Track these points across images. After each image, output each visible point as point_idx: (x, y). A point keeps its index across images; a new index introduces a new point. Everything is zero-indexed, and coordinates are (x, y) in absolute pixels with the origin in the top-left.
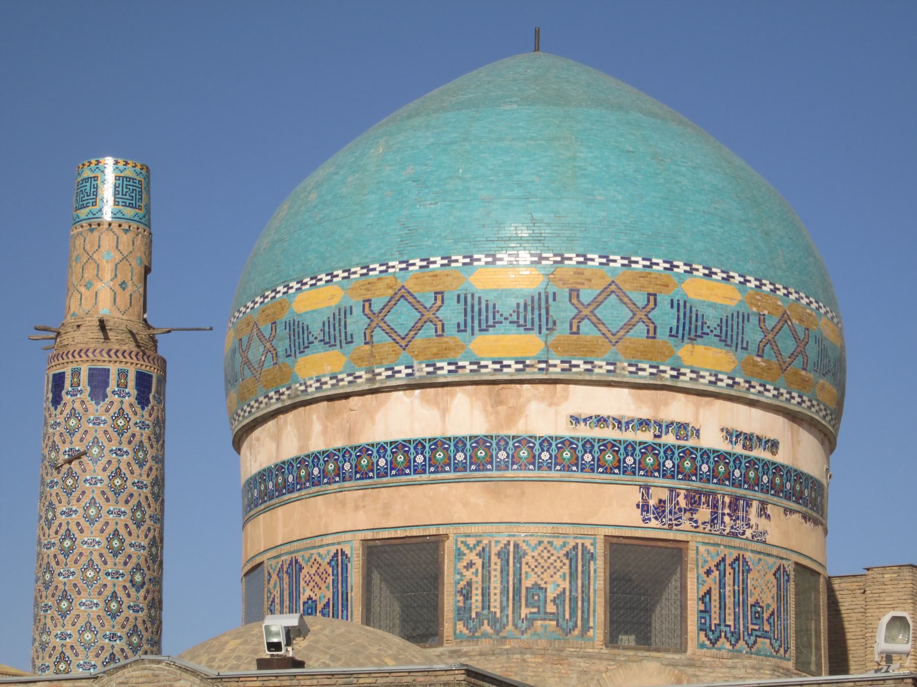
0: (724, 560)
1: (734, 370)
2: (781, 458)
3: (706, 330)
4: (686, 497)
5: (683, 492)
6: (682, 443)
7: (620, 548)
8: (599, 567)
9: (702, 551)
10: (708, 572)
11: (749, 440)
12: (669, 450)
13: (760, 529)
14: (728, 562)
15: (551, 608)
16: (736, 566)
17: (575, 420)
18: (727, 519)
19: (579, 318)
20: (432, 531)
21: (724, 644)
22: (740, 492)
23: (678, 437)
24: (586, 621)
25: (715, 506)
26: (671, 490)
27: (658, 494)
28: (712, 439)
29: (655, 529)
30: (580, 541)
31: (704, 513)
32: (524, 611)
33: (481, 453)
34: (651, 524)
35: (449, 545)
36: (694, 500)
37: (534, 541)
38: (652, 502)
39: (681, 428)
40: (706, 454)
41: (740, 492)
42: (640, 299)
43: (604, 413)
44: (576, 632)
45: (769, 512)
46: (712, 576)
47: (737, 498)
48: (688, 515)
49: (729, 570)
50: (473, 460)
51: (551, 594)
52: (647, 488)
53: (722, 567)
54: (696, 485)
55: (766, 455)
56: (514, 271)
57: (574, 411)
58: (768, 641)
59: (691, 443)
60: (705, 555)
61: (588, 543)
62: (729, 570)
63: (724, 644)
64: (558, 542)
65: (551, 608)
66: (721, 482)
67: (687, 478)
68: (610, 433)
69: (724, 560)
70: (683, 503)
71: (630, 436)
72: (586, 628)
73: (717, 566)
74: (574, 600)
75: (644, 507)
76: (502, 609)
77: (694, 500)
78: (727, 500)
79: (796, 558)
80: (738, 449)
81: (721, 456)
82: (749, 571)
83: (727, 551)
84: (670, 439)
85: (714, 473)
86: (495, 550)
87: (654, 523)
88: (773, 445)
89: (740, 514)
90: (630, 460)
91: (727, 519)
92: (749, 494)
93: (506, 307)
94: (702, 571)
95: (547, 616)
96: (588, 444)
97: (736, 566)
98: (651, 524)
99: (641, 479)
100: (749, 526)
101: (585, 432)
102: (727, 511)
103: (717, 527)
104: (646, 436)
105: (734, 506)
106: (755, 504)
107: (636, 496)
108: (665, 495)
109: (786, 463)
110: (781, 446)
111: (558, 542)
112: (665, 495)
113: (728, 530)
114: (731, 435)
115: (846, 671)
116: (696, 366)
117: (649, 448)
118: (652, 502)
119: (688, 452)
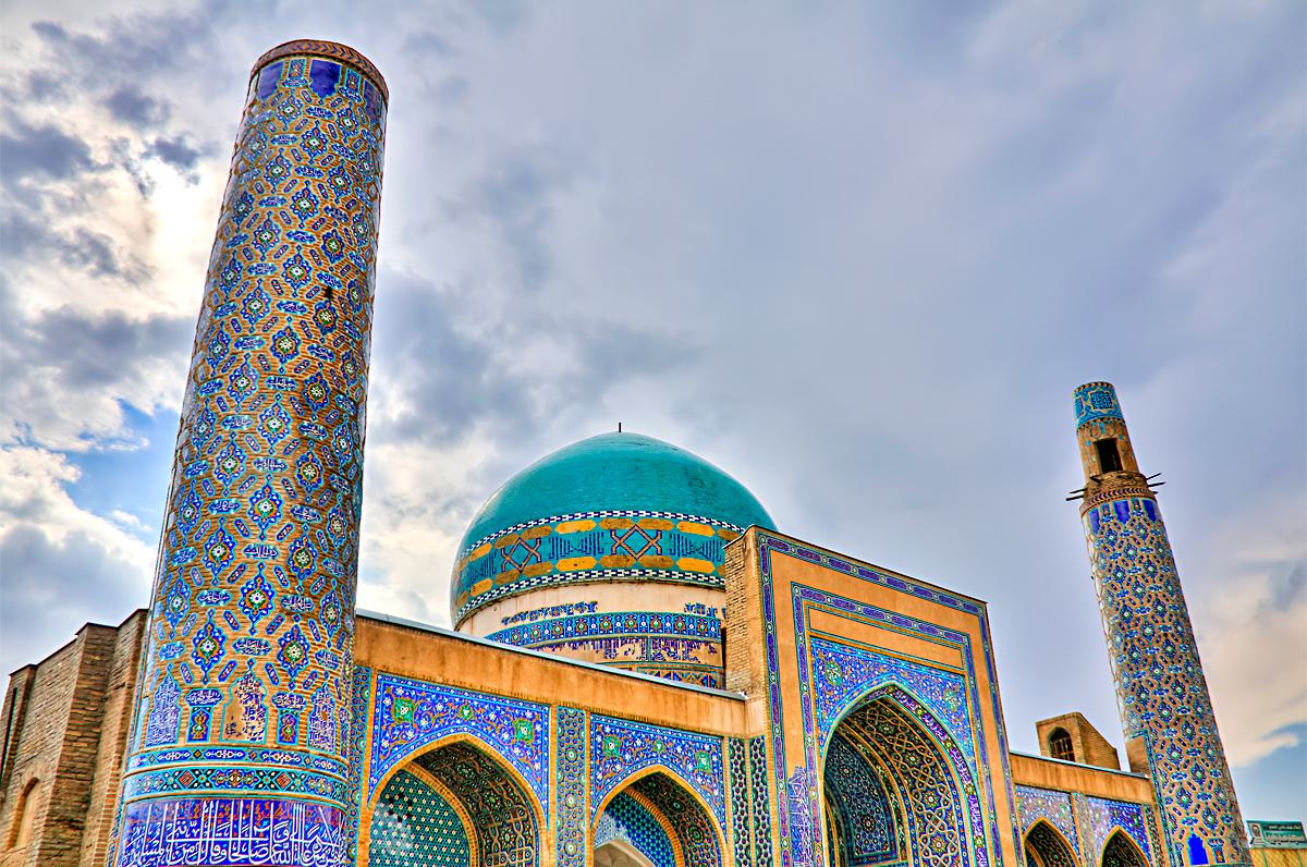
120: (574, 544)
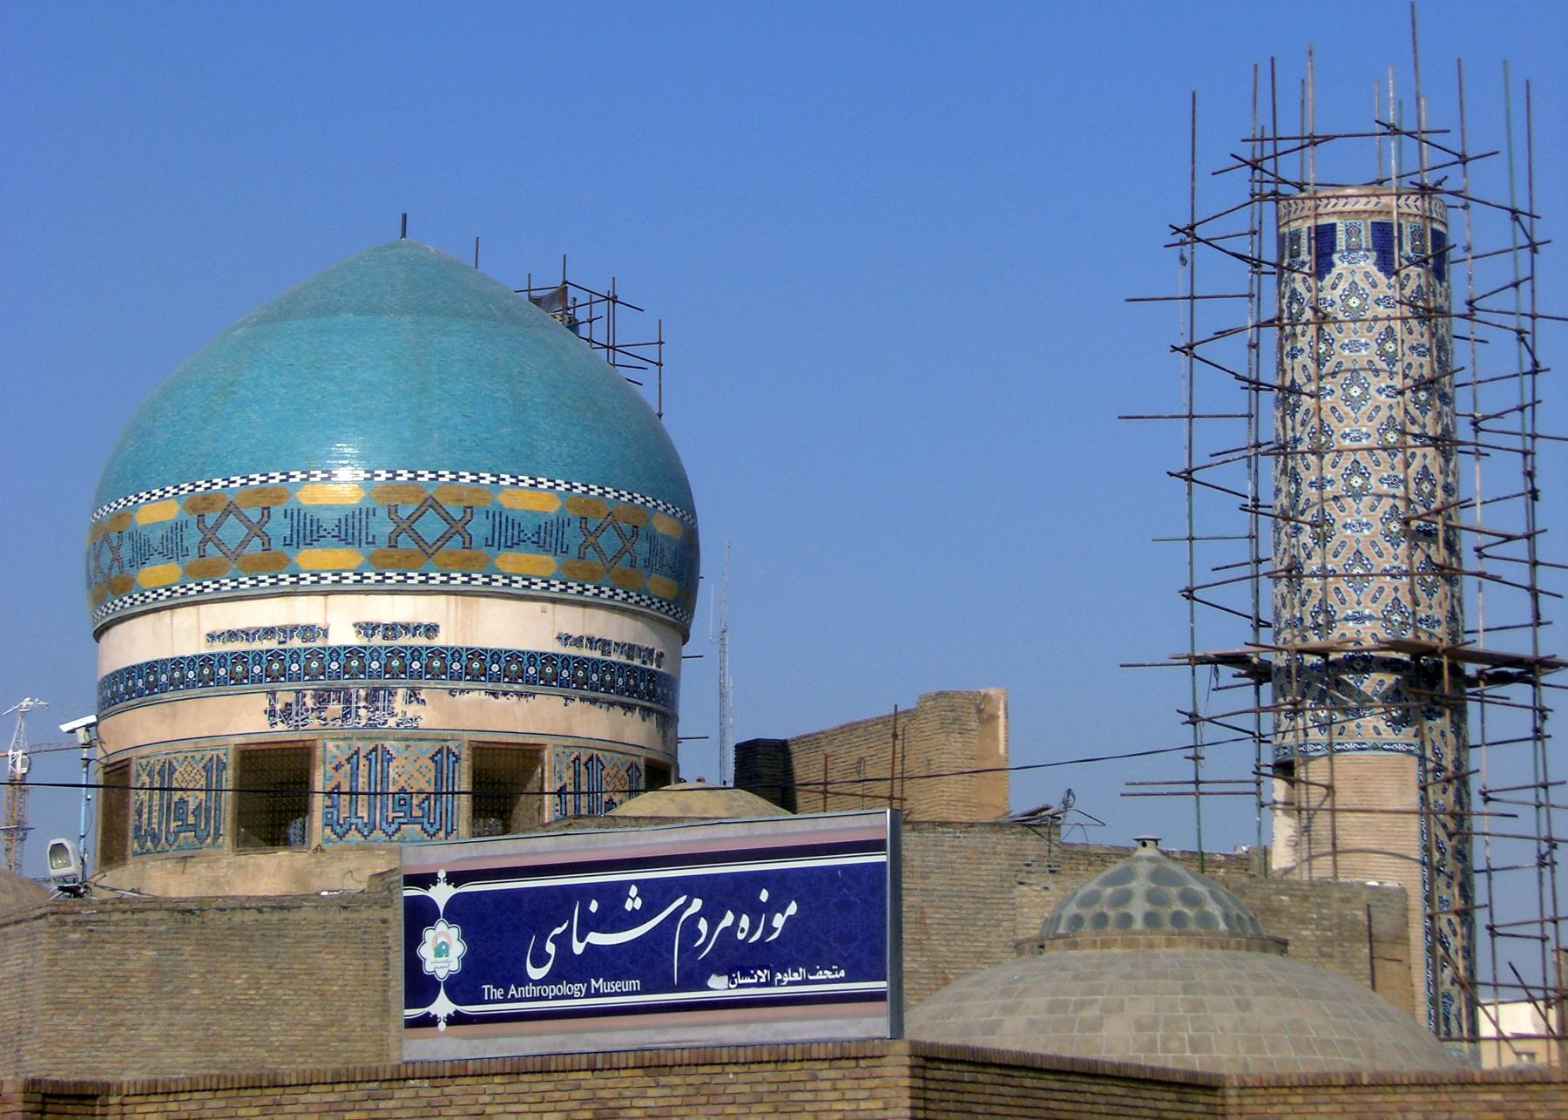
0: (357, 753)
1: (361, 567)
2: (440, 641)
3: (322, 533)
4: (314, 697)
6: (309, 645)
7: (253, 758)
8: (465, 767)
9: (331, 750)
10: (337, 768)
11: (392, 630)
13: (409, 715)
14: (362, 754)
17: (212, 637)
18: (362, 712)
19: (204, 542)
20: (532, 740)
21: (354, 837)
22: (378, 683)
23: (305, 640)
24: (217, 829)
25: (348, 701)
26: (297, 692)
27: (284, 698)
28: (343, 635)
29: (282, 731)
31: (335, 708)
32: (173, 825)
33: (436, 664)
34: (277, 728)
36: (322, 699)
37: (181, 757)
38: (279, 707)
39: (308, 631)
40: (335, 652)
41: (378, 683)
44: (209, 840)
45: (422, 697)
46: (342, 771)
47: (376, 690)
48: (316, 714)
49: (363, 762)
50: (428, 669)
51: (192, 807)
52: (273, 693)
53: (354, 760)
57: (209, 628)
58: (418, 827)
59: (319, 643)
60: (334, 750)
61: (221, 753)
62: (363, 762)
63: (354, 837)
65: (191, 820)
66: (354, 676)
67: (314, 678)
68: (239, 646)
69: (357, 753)
70: (310, 702)
71: (257, 645)
72: (217, 835)
73: (348, 760)
74: (208, 810)
75: (272, 713)
76: (160, 824)
77: (322, 699)
78: (362, 693)
79: (467, 737)
80: (377, 640)
81: (354, 652)
82: (389, 760)
83: (360, 744)
84: (296, 643)
86: (157, 768)
87: (280, 727)
88: (432, 630)
89: (380, 705)
91: (362, 712)
92: (392, 683)
94: (329, 767)
98: (277, 728)
100: (392, 714)
101: (220, 647)
102: (362, 704)
103: (350, 722)
104: (271, 644)
105: (372, 697)
106: (401, 692)
107: (263, 702)
108: (291, 698)
109: (451, 644)
110: (441, 629)
111: (198, 756)
112: (291, 698)
113: (363, 722)
114: (367, 629)
116: (316, 569)
117: (275, 655)
118: (279, 707)
119: (315, 653)
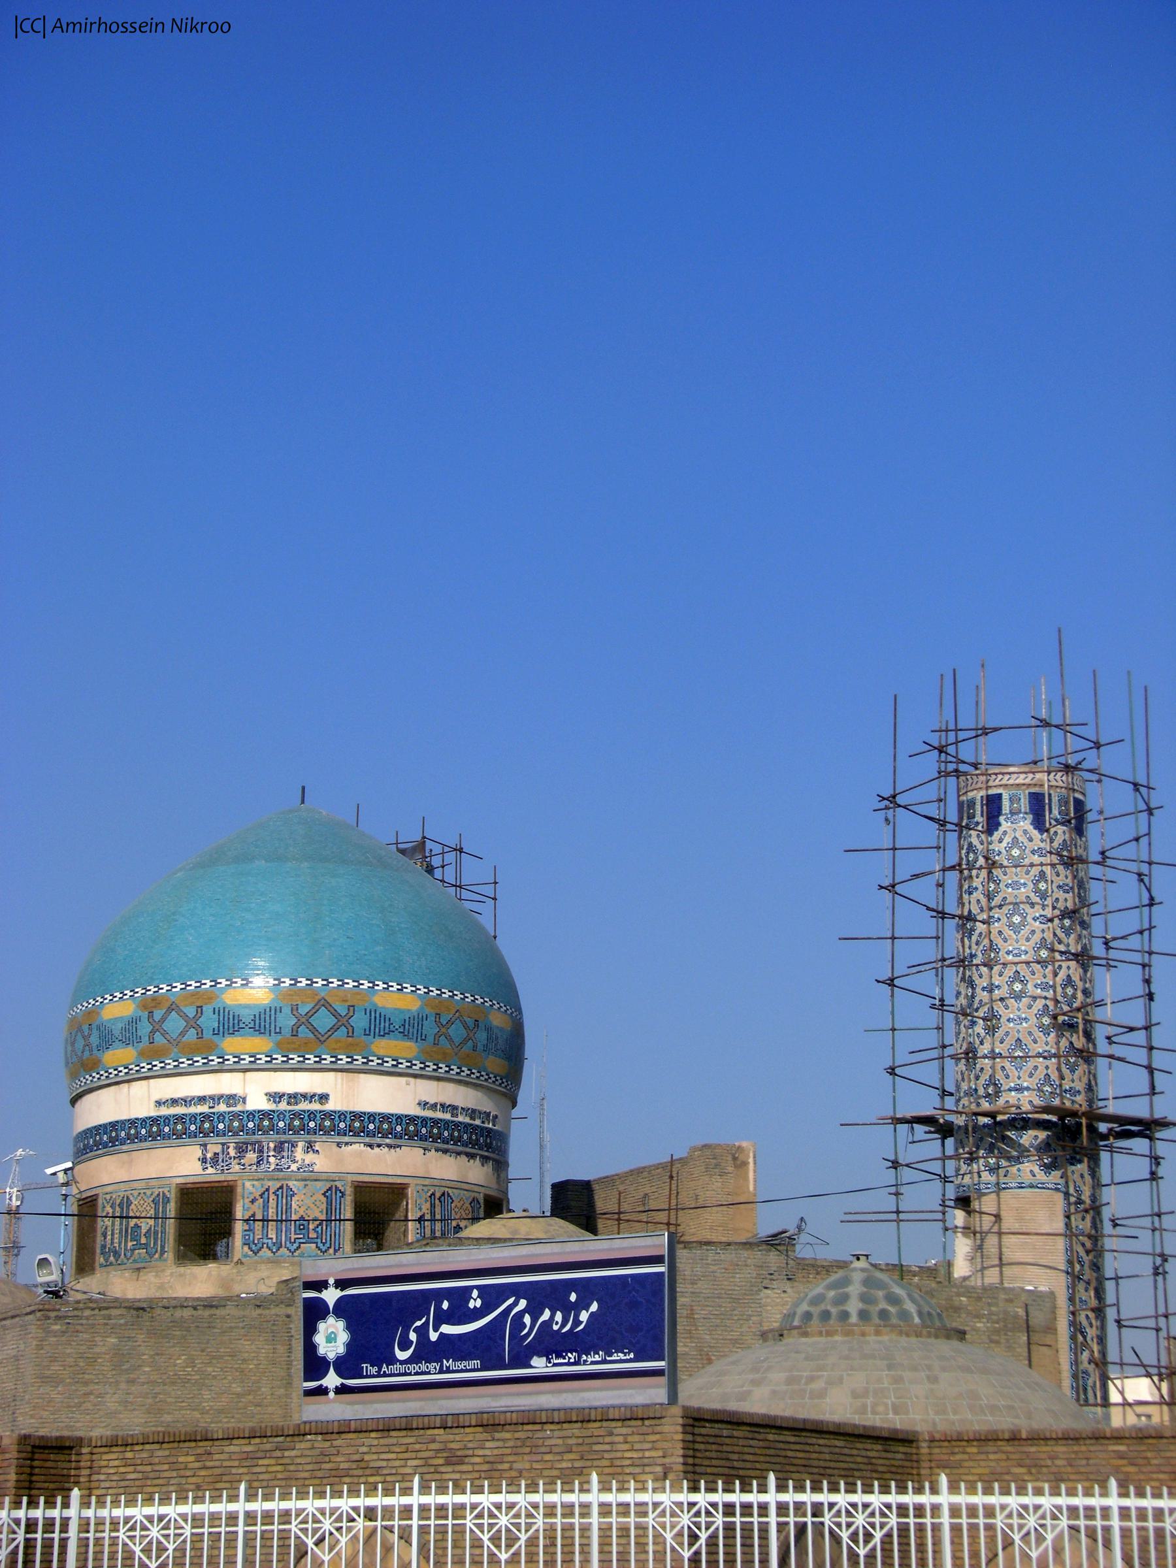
0: (267, 1190)
2: (330, 1106)
3: (242, 1025)
4: (235, 1148)
5: (232, 1145)
6: (231, 1109)
8: (349, 1200)
9: (248, 1188)
10: (253, 1202)
11: (294, 1098)
12: (221, 1116)
13: (307, 1162)
14: (271, 1191)
15: (143, 1240)
16: (279, 1193)
17: (159, 1103)
18: (272, 1159)
19: (153, 1032)
20: (399, 1180)
22: (283, 1138)
23: (229, 1105)
24: (163, 1247)
25: (261, 1151)
26: (223, 1144)
27: (213, 1149)
28: (257, 1102)
29: (211, 1174)
30: (285, 1183)
31: (251, 1156)
32: (130, 1244)
34: (208, 1172)
35: (100, 1201)
36: (241, 1150)
37: (135, 1193)
38: (209, 1155)
39: (231, 1099)
40: (251, 1115)
42: (191, 1011)
43: (176, 1096)
44: (157, 1256)
45: (317, 1148)
46: (256, 1204)
48: (237, 1161)
50: (321, 1127)
51: (144, 1231)
52: (205, 1145)
54: (243, 1137)
55: (315, 1106)
56: (257, 989)
57: (157, 1097)
59: (239, 1108)
60: (251, 1188)
62: (272, 1197)
63: (265, 1253)
64: (149, 1192)
67: (236, 1134)
68: (179, 1110)
69: (267, 1190)
70: (232, 1152)
71: (193, 1110)
73: (261, 1196)
74: (156, 1233)
75: (204, 1160)
76: (120, 1243)
77: (241, 1150)
78: (272, 1145)
80: (283, 1106)
81: (265, 1114)
82: (292, 1196)
84: (222, 1108)
85: (260, 1128)
86: (118, 1201)
87: (210, 1170)
88: (324, 1098)
90: (221, 1126)
91: (272, 1159)
92: (294, 1138)
93: (247, 1019)
94: (247, 1201)
95: (310, 1241)
96: (167, 1119)
97: (279, 1193)
98: (208, 1172)
99: (201, 1139)
100: (294, 1161)
101: (165, 1111)
102: (272, 1153)
104: (203, 1109)
105: (279, 1148)
107: (197, 1152)
108: (218, 1149)
109: (338, 1108)
110: (331, 1097)
112: (218, 1149)
113: (273, 1167)
114: (276, 1097)
115: (663, 1256)
116: (237, 1052)
117: (206, 1117)
118: (209, 1155)
119: (236, 1116)
120: (117, 1033)
